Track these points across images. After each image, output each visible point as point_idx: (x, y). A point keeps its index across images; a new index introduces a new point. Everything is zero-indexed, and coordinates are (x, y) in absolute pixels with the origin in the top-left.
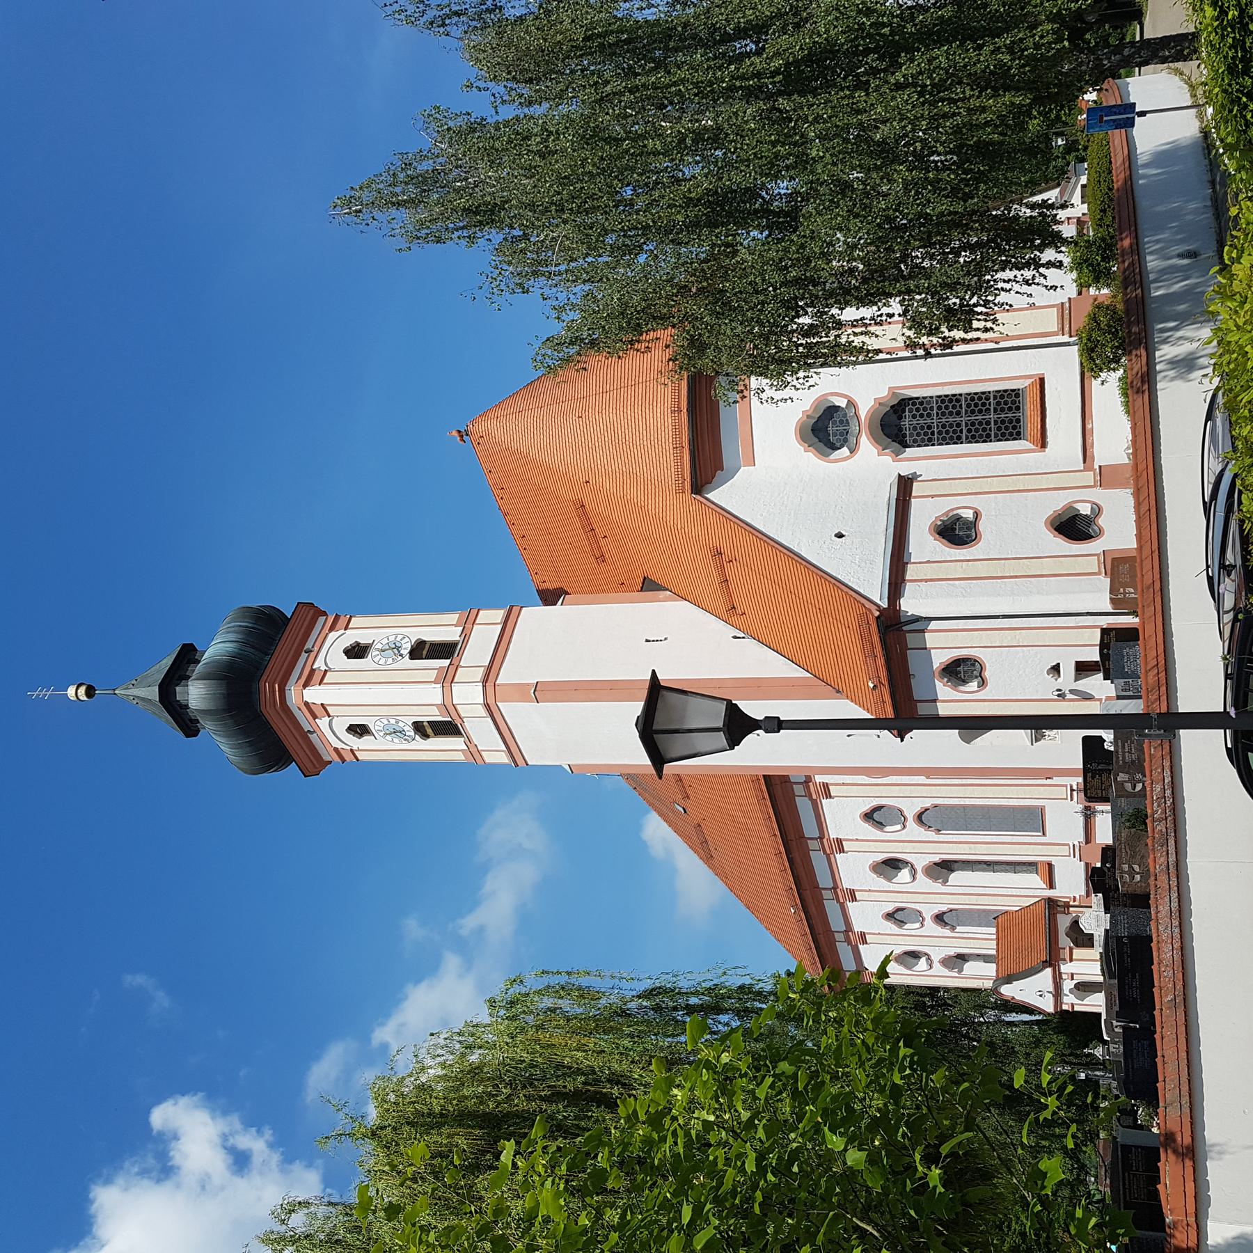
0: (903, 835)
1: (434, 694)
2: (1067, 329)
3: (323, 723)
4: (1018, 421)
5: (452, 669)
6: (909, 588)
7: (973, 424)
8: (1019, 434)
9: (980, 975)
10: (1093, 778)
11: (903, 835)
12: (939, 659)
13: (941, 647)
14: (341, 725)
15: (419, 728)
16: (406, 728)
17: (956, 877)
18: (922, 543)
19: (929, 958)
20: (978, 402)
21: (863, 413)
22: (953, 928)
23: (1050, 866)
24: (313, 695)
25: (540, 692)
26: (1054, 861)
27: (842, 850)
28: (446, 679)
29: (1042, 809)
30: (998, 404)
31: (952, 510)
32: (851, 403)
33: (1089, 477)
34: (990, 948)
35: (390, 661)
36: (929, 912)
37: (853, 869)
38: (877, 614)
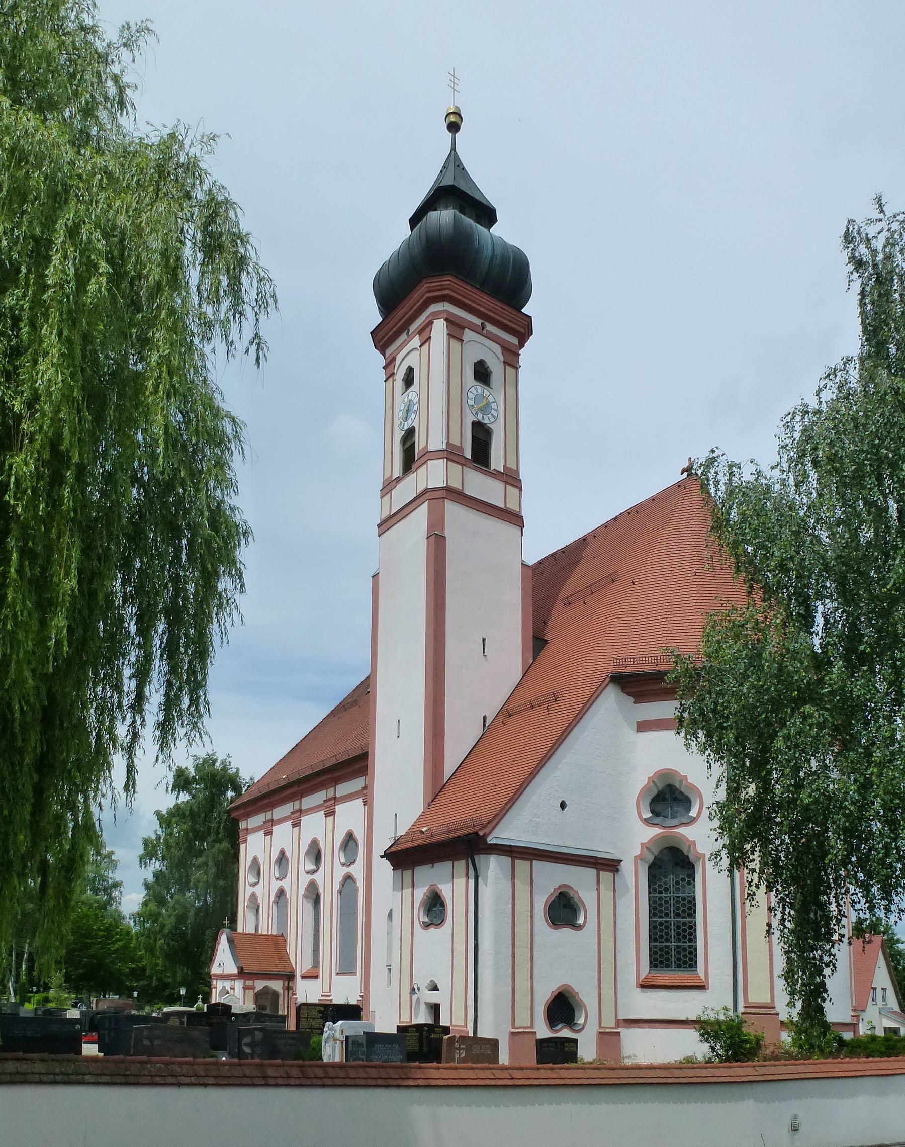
0: (337, 863)
1: (437, 442)
2: (749, 1010)
3: (416, 342)
4: (668, 966)
5: (463, 461)
6: (507, 860)
7: (667, 927)
8: (656, 966)
9: (246, 923)
10: (320, 1012)
11: (337, 863)
12: (445, 890)
13: (454, 887)
14: (413, 360)
15: (410, 433)
16: (410, 422)
17: (309, 906)
18: (551, 878)
19: (256, 884)
20: (688, 933)
21: (682, 830)
22: (274, 902)
23: (316, 977)
24: (440, 328)
25: (437, 542)
26: (320, 980)
27: (327, 815)
28: (451, 454)
29: (354, 973)
30: (685, 950)
31: (584, 906)
32: (693, 820)
33: (609, 1023)
34: (263, 930)
35: (471, 403)
36: (285, 884)
37: (314, 825)
38: (481, 833)
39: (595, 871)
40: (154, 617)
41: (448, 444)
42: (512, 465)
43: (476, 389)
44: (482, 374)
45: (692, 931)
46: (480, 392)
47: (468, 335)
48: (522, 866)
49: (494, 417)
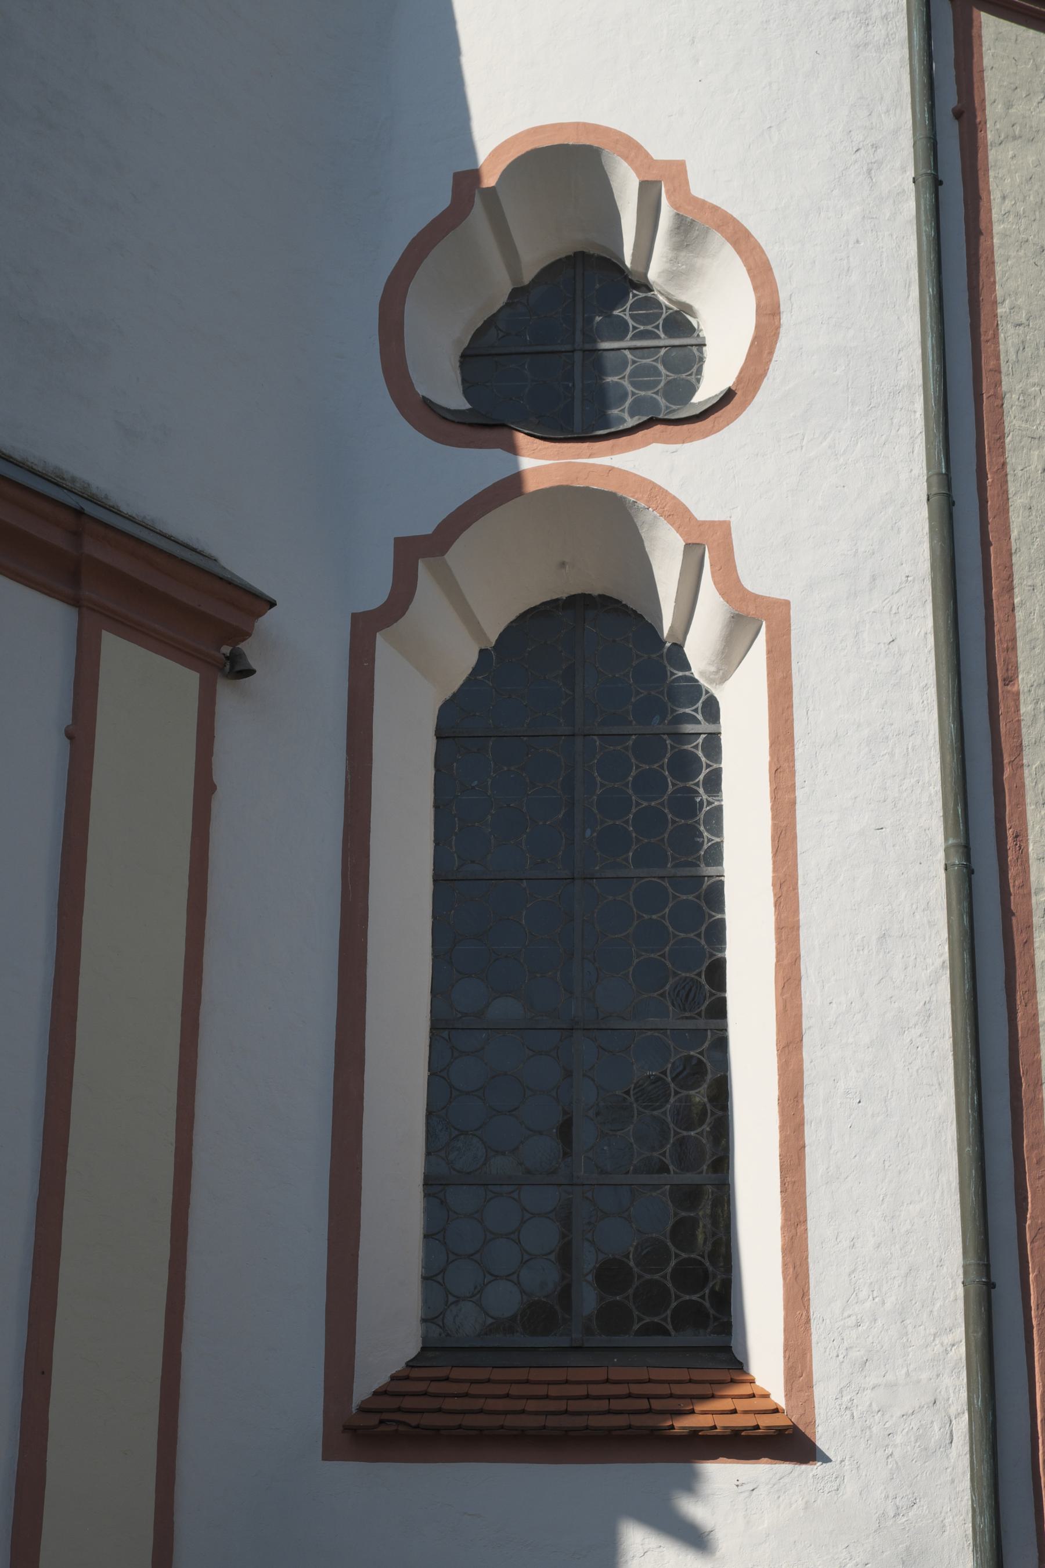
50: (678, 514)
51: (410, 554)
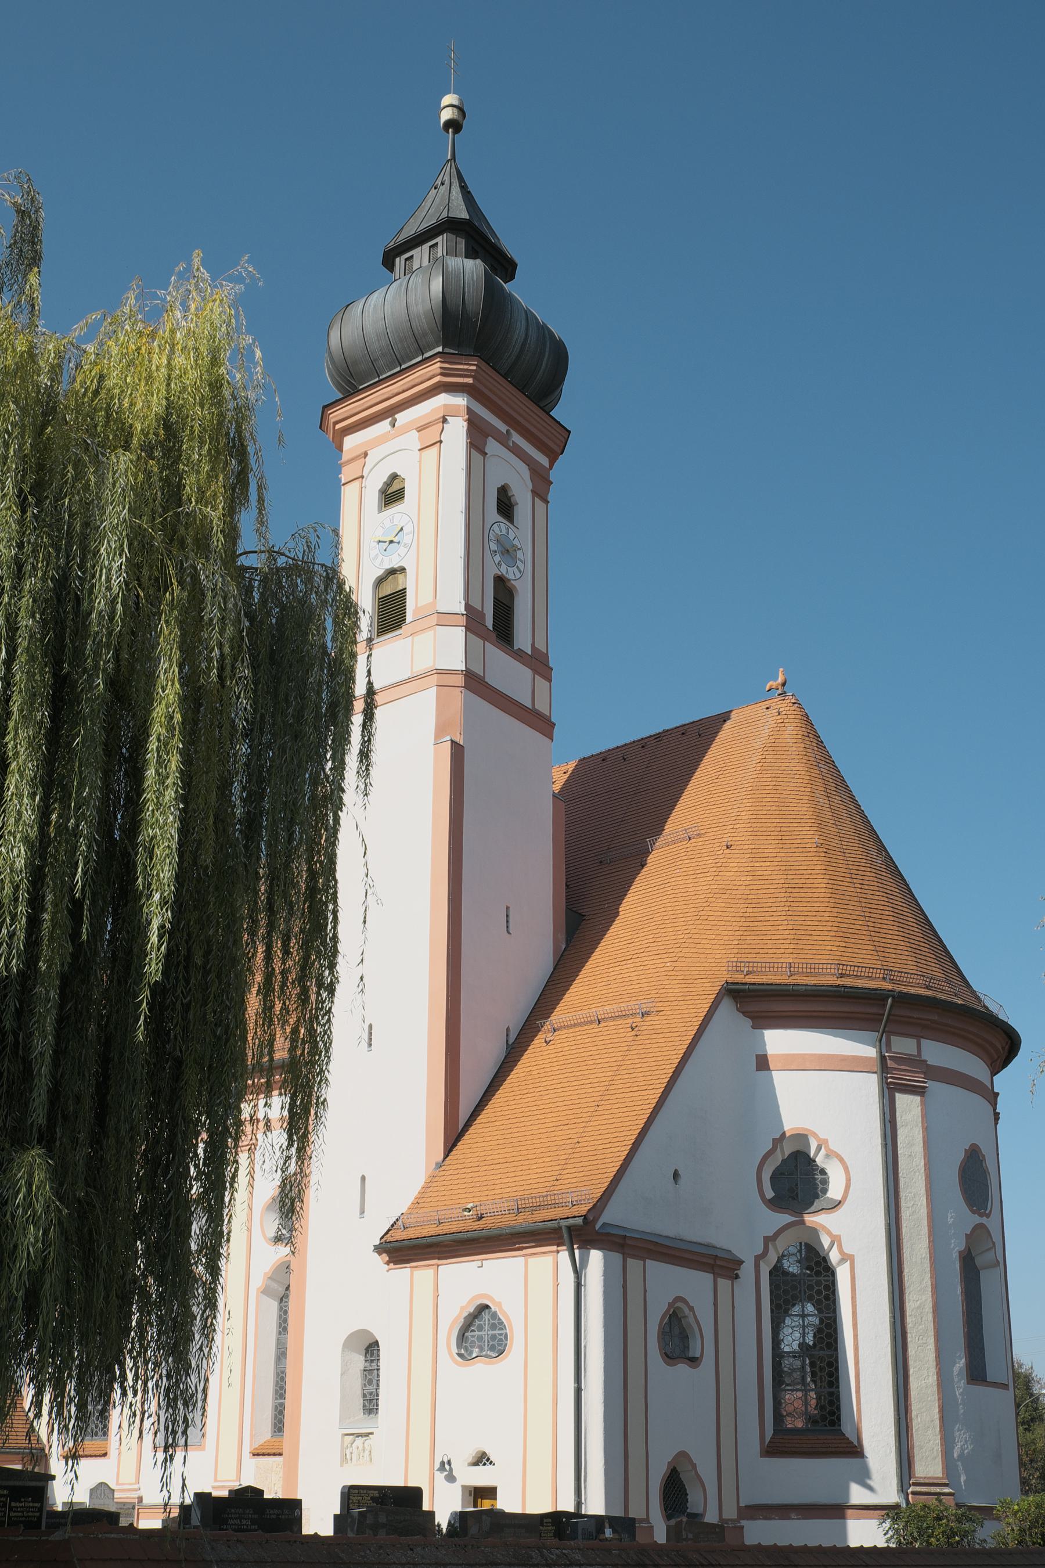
18: (668, 1283)
39: (708, 1277)
40: (85, 785)
41: (467, 606)
42: (540, 646)
43: (499, 526)
44: (506, 507)
45: (834, 1418)
46: (504, 532)
47: (492, 446)
48: (634, 1264)
49: (520, 571)
50: (829, 1233)
51: (767, 1240)
